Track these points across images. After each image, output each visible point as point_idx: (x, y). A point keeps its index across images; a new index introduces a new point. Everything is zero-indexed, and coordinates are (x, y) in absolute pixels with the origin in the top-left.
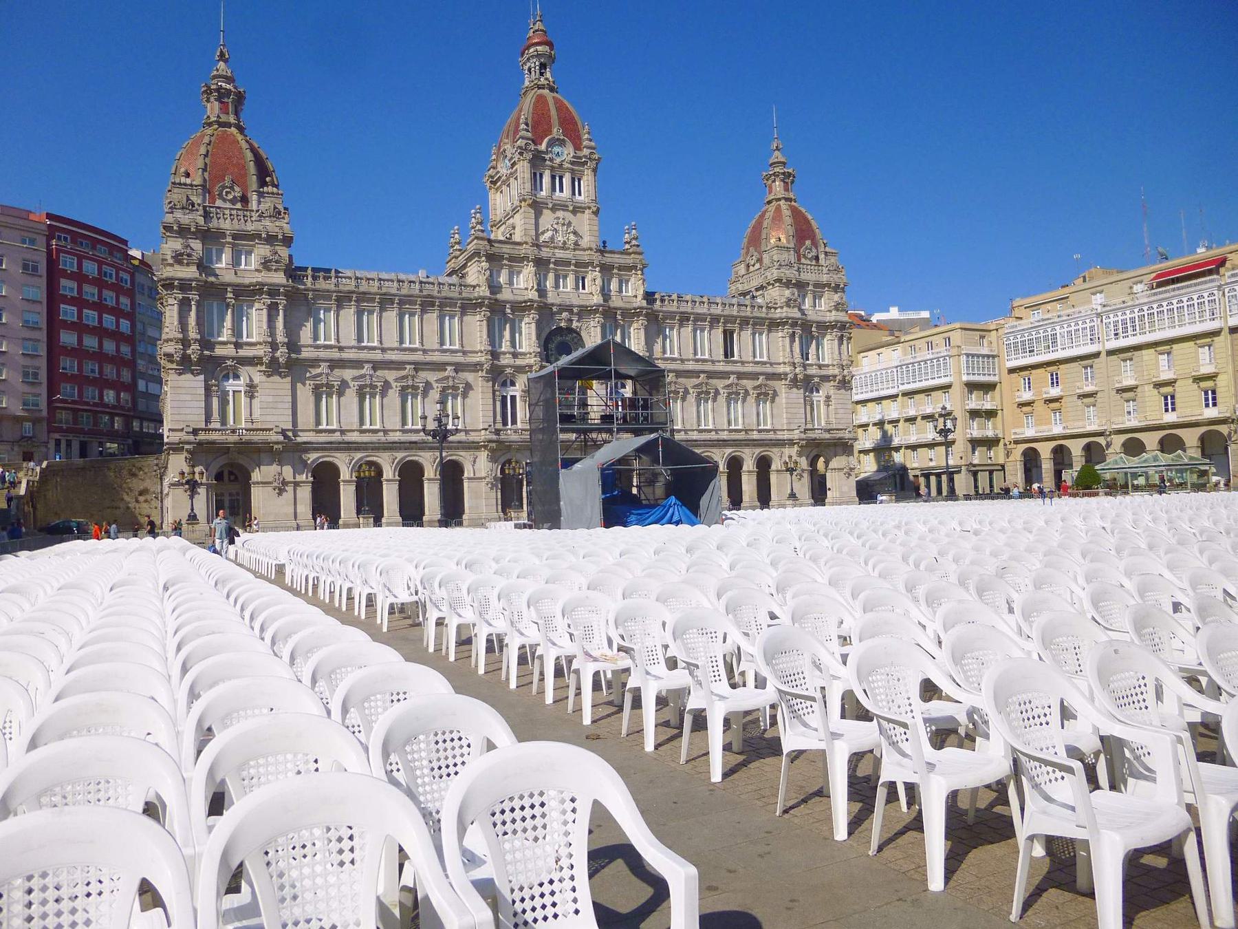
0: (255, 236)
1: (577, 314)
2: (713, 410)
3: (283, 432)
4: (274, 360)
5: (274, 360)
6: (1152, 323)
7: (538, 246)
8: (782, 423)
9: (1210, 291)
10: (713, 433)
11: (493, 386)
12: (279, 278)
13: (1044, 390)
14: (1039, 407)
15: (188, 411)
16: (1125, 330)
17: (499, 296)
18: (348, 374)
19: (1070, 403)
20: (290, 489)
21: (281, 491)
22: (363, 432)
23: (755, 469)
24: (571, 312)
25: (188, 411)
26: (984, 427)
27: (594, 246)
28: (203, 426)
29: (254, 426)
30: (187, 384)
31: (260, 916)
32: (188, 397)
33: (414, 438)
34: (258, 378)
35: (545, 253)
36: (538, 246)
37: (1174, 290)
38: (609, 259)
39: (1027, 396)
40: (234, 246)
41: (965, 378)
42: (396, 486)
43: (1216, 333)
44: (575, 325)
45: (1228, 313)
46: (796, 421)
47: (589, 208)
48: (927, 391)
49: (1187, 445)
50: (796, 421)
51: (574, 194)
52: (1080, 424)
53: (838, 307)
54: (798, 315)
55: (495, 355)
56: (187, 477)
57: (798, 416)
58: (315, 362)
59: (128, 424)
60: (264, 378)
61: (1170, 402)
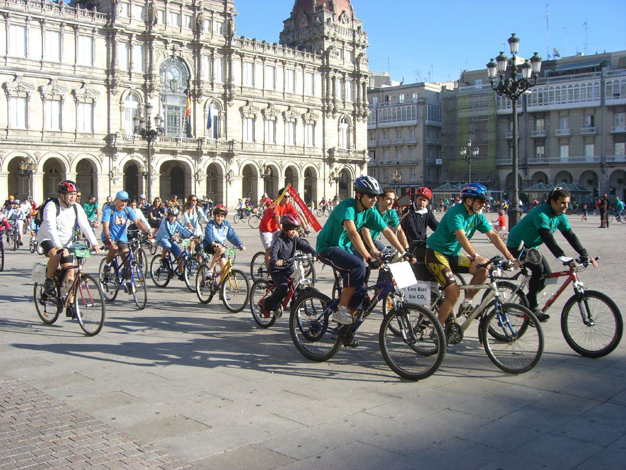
24: (181, 45)
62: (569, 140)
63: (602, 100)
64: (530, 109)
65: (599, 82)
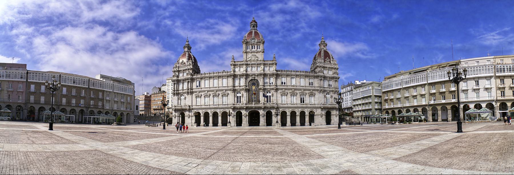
0: (332, 68)
1: (257, 76)
2: (296, 99)
3: (189, 106)
4: (188, 92)
5: (188, 92)
6: (412, 82)
7: (247, 61)
8: (316, 102)
9: (416, 76)
10: (305, 105)
11: (234, 94)
12: (189, 76)
13: (390, 97)
14: (418, 97)
15: (175, 103)
16: (407, 83)
17: (236, 73)
18: (202, 93)
19: (411, 99)
20: (191, 117)
21: (189, 118)
22: (205, 105)
23: (308, 114)
24: (255, 75)
25: (175, 103)
26: (369, 106)
27: (262, 60)
28: (177, 105)
29: (186, 105)
30: (175, 98)
31: (249, 126)
32: (175, 100)
33: (216, 106)
34: (186, 96)
35: (249, 63)
36: (247, 61)
37: (422, 73)
38: (266, 62)
39: (415, 94)
40: (183, 72)
41: (374, 94)
42: (212, 117)
43: (425, 85)
44: (256, 78)
46: (321, 102)
47: (261, 51)
48: (367, 97)
49: (419, 111)
50: (321, 102)
51: (258, 49)
52: (390, 106)
53: (334, 73)
54: (323, 75)
55: (234, 86)
56: (276, 113)
57: (322, 100)
58: (196, 92)
59: (74, 97)
60: (187, 96)
61: (503, 94)
64: (429, 82)
65: (59, 76)
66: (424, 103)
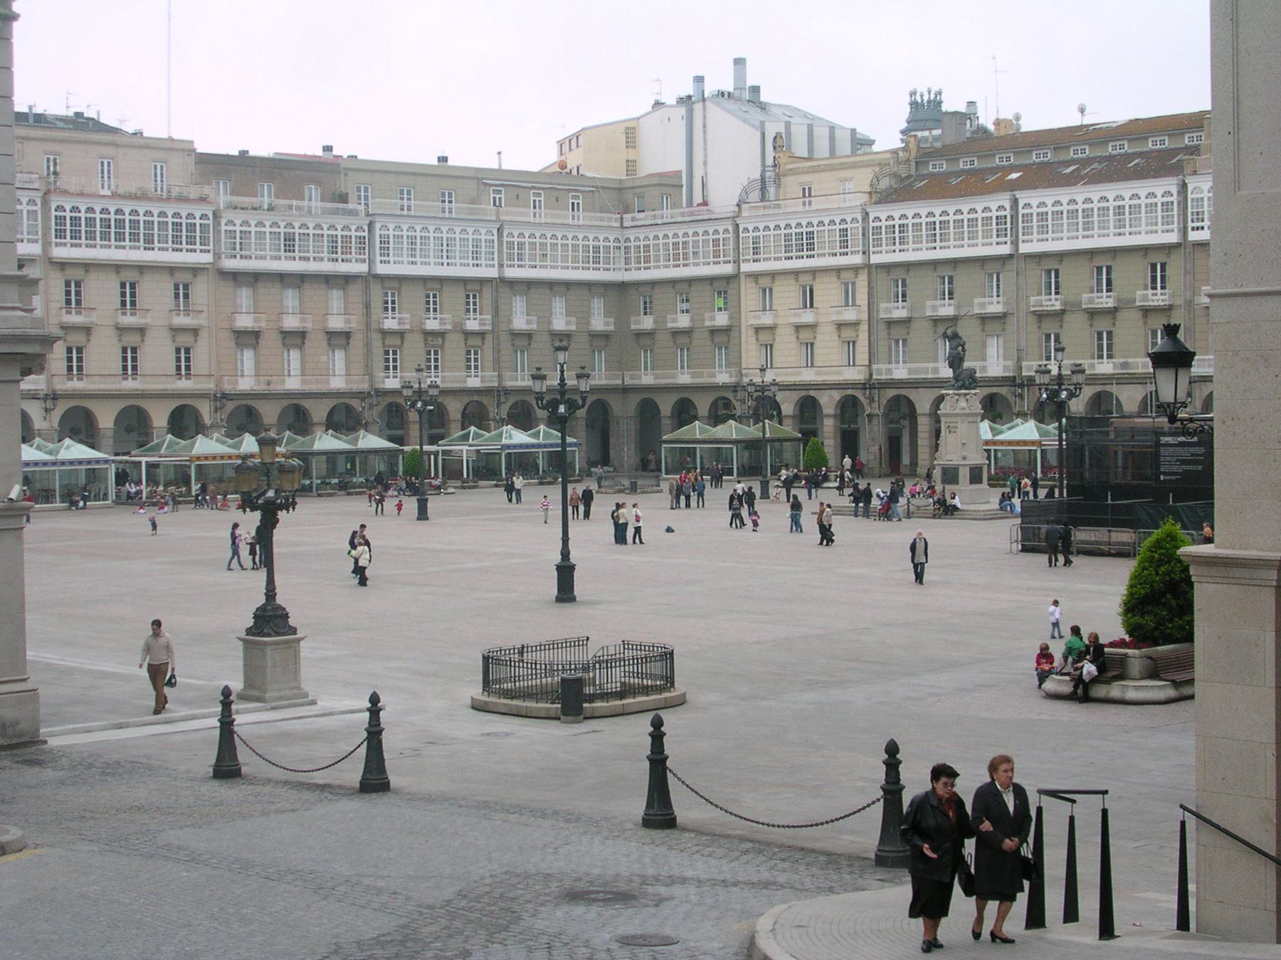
45: (1021, 237)
62: (857, 330)
63: (1015, 243)
64: (875, 259)
66: (474, 382)
